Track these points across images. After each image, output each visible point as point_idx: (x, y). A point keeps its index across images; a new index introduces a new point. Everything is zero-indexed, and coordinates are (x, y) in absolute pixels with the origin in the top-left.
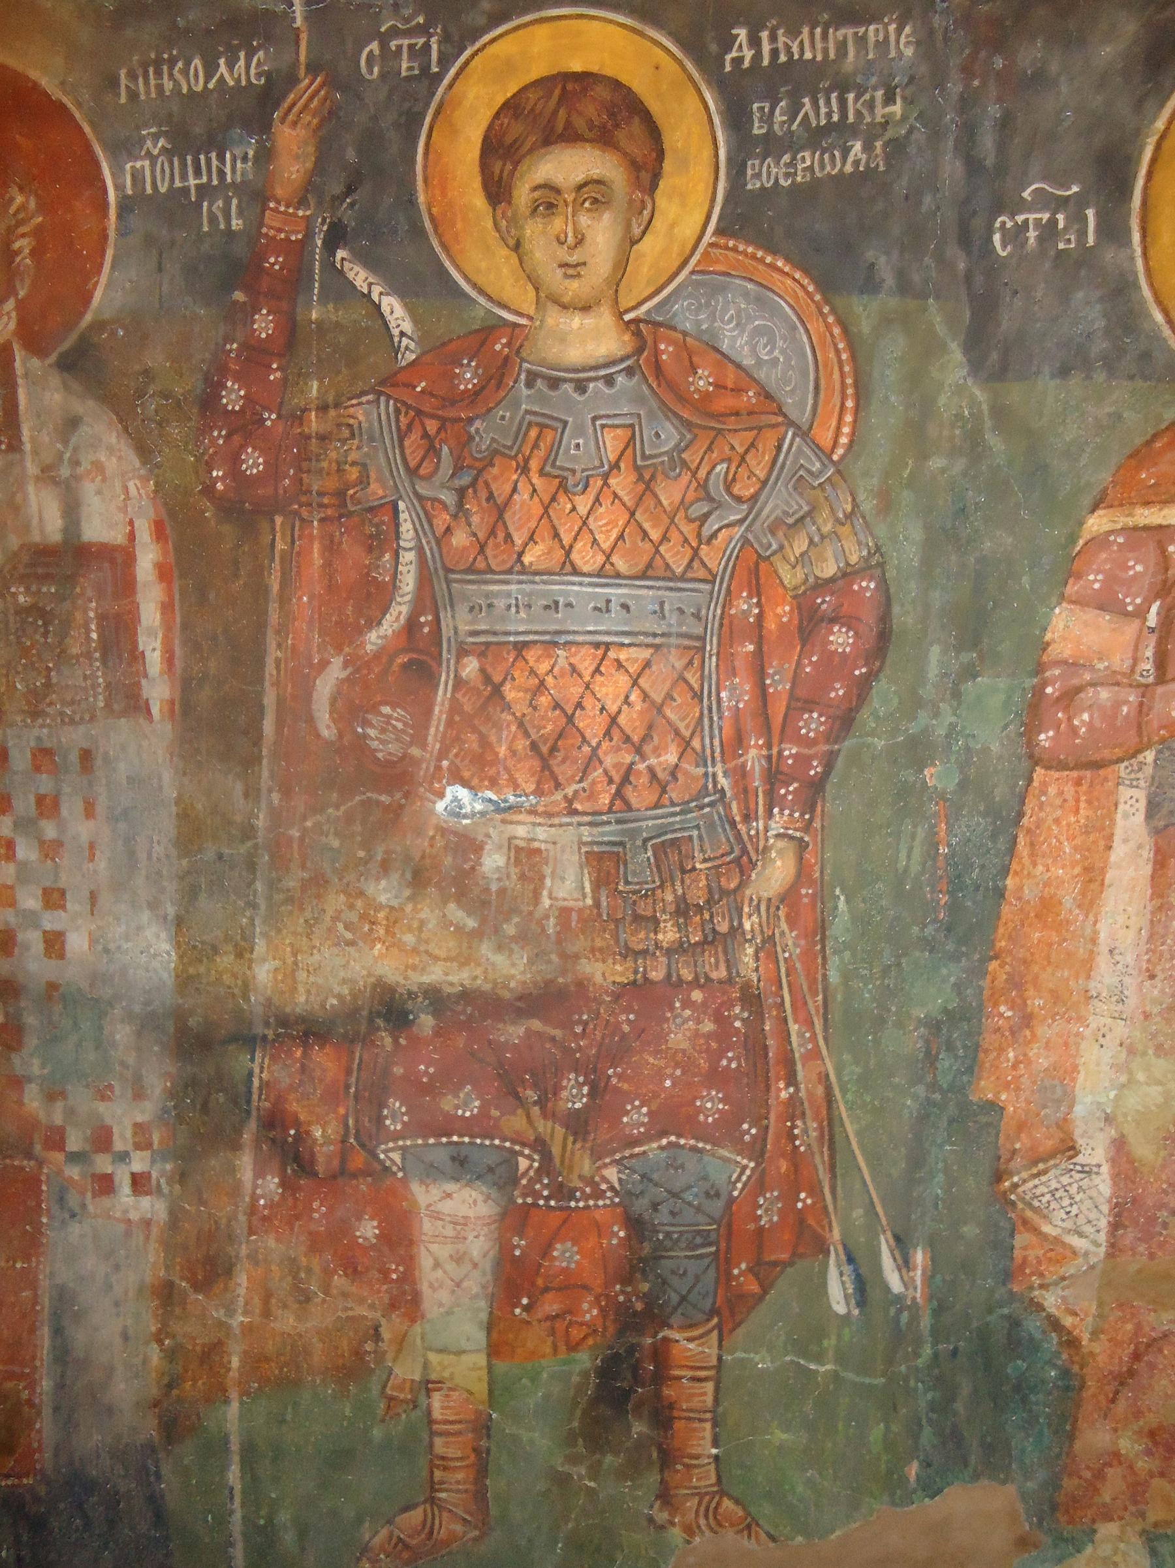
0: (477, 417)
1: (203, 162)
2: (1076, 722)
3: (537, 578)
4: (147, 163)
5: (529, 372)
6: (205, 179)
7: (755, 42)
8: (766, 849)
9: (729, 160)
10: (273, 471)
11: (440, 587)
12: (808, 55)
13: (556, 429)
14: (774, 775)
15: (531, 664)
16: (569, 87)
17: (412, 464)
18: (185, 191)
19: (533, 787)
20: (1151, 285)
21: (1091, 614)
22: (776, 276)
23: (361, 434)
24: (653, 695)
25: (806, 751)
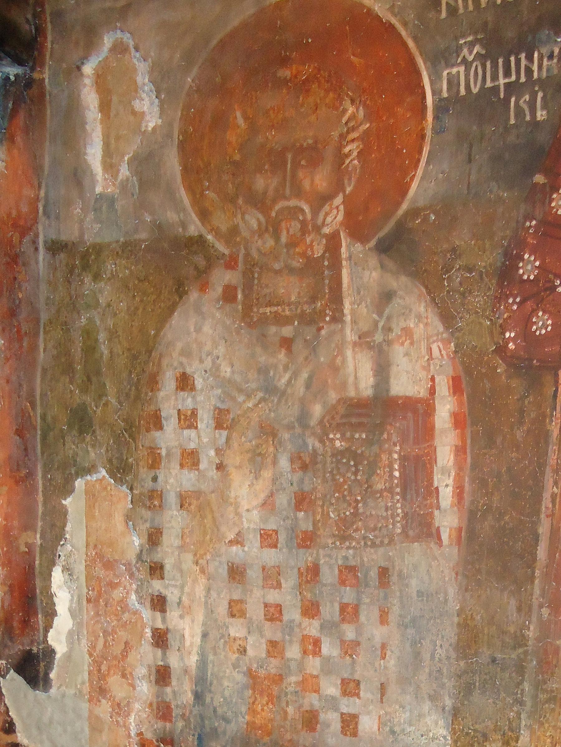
4: (462, 69)
6: (513, 78)
18: (495, 89)
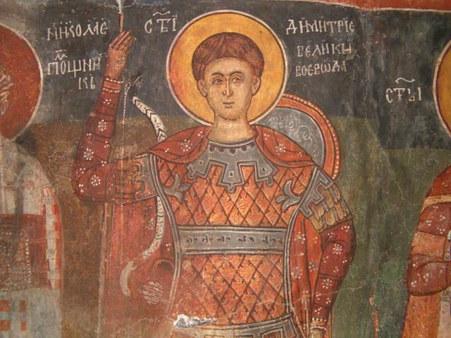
0: (191, 163)
1: (80, 63)
2: (424, 277)
3: (215, 228)
4: (57, 63)
5: (211, 144)
6: (80, 69)
7: (297, 25)
8: (310, 334)
9: (289, 66)
10: (105, 184)
11: (174, 232)
12: (317, 30)
13: (222, 167)
14: (312, 305)
15: (213, 263)
16: (227, 37)
17: (163, 182)
18: (72, 74)
19: (214, 314)
20: (442, 115)
21: (427, 236)
22: (308, 108)
23: (142, 169)
24: (264, 275)
25: (324, 294)
